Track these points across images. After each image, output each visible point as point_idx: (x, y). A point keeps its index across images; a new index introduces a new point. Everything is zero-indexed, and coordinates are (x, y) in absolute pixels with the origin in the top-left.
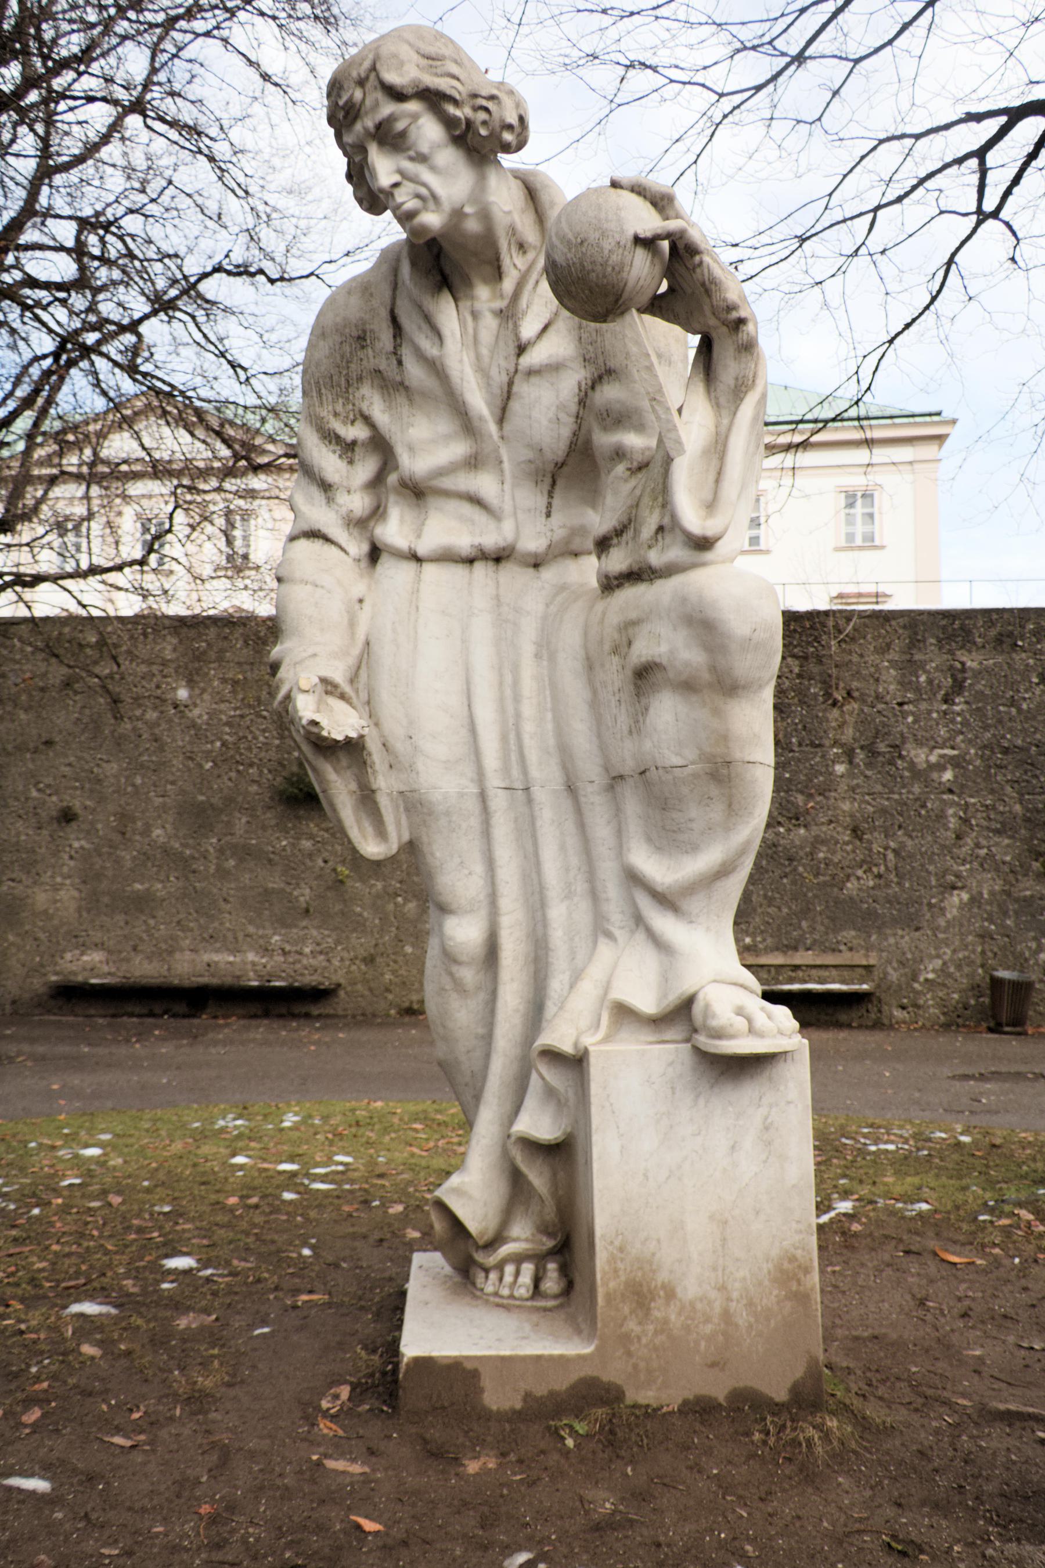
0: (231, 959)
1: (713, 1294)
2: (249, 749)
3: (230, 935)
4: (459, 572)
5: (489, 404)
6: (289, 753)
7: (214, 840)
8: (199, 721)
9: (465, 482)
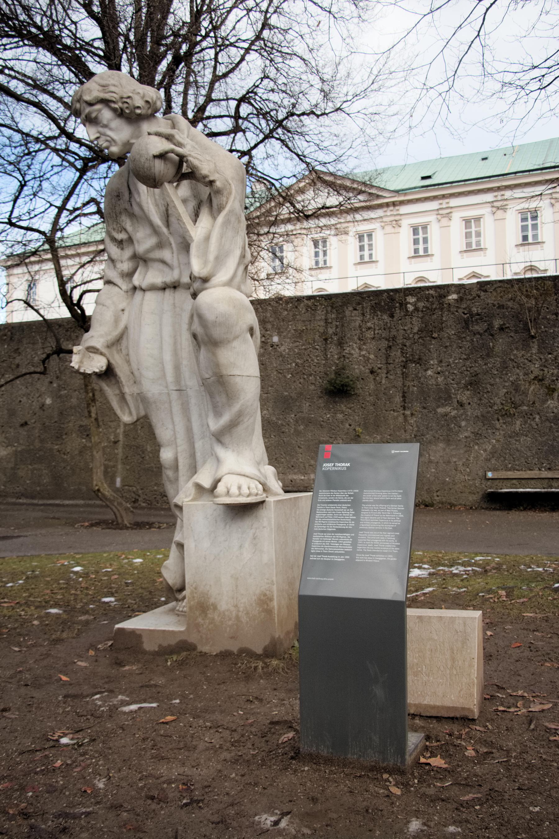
0: (303, 478)
1: (232, 609)
2: (310, 367)
3: (302, 465)
4: (160, 294)
5: (161, 220)
6: (330, 368)
7: (293, 416)
8: (284, 353)
9: (157, 254)
